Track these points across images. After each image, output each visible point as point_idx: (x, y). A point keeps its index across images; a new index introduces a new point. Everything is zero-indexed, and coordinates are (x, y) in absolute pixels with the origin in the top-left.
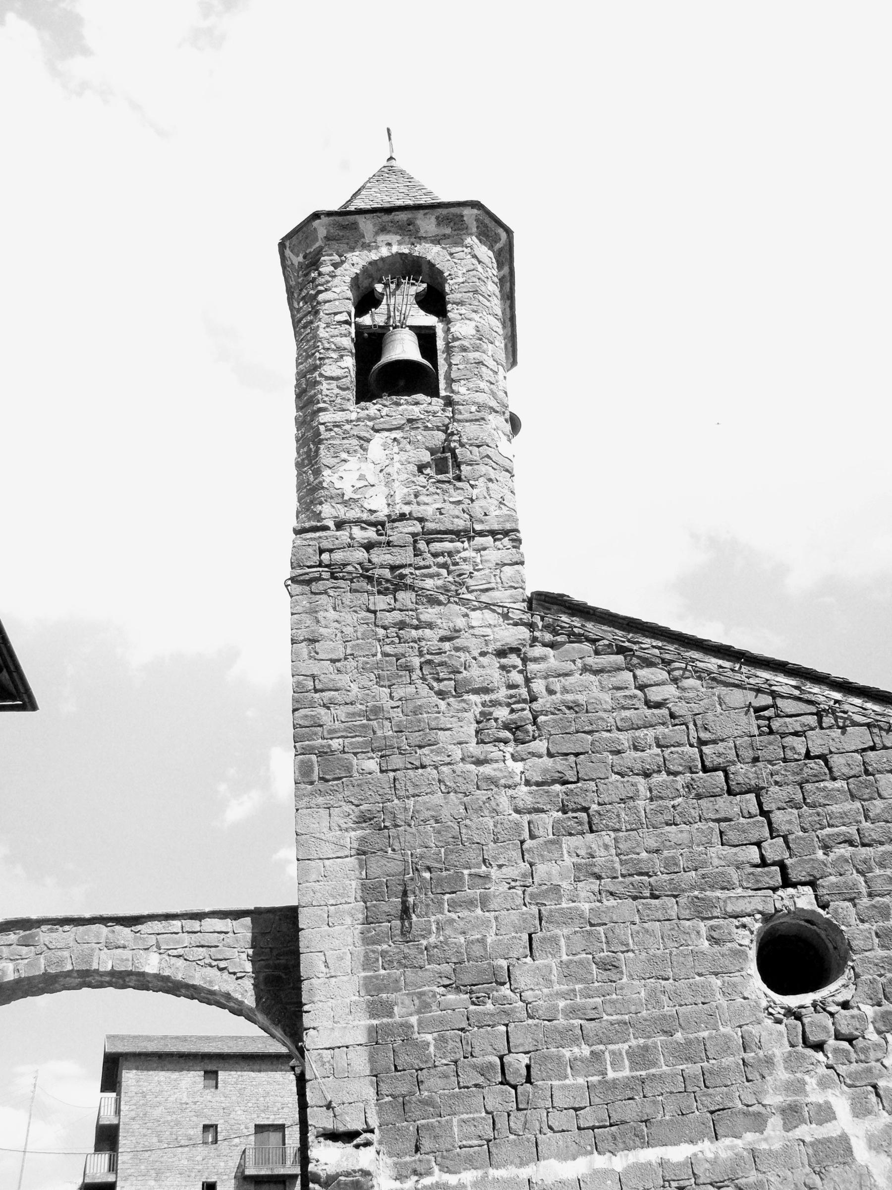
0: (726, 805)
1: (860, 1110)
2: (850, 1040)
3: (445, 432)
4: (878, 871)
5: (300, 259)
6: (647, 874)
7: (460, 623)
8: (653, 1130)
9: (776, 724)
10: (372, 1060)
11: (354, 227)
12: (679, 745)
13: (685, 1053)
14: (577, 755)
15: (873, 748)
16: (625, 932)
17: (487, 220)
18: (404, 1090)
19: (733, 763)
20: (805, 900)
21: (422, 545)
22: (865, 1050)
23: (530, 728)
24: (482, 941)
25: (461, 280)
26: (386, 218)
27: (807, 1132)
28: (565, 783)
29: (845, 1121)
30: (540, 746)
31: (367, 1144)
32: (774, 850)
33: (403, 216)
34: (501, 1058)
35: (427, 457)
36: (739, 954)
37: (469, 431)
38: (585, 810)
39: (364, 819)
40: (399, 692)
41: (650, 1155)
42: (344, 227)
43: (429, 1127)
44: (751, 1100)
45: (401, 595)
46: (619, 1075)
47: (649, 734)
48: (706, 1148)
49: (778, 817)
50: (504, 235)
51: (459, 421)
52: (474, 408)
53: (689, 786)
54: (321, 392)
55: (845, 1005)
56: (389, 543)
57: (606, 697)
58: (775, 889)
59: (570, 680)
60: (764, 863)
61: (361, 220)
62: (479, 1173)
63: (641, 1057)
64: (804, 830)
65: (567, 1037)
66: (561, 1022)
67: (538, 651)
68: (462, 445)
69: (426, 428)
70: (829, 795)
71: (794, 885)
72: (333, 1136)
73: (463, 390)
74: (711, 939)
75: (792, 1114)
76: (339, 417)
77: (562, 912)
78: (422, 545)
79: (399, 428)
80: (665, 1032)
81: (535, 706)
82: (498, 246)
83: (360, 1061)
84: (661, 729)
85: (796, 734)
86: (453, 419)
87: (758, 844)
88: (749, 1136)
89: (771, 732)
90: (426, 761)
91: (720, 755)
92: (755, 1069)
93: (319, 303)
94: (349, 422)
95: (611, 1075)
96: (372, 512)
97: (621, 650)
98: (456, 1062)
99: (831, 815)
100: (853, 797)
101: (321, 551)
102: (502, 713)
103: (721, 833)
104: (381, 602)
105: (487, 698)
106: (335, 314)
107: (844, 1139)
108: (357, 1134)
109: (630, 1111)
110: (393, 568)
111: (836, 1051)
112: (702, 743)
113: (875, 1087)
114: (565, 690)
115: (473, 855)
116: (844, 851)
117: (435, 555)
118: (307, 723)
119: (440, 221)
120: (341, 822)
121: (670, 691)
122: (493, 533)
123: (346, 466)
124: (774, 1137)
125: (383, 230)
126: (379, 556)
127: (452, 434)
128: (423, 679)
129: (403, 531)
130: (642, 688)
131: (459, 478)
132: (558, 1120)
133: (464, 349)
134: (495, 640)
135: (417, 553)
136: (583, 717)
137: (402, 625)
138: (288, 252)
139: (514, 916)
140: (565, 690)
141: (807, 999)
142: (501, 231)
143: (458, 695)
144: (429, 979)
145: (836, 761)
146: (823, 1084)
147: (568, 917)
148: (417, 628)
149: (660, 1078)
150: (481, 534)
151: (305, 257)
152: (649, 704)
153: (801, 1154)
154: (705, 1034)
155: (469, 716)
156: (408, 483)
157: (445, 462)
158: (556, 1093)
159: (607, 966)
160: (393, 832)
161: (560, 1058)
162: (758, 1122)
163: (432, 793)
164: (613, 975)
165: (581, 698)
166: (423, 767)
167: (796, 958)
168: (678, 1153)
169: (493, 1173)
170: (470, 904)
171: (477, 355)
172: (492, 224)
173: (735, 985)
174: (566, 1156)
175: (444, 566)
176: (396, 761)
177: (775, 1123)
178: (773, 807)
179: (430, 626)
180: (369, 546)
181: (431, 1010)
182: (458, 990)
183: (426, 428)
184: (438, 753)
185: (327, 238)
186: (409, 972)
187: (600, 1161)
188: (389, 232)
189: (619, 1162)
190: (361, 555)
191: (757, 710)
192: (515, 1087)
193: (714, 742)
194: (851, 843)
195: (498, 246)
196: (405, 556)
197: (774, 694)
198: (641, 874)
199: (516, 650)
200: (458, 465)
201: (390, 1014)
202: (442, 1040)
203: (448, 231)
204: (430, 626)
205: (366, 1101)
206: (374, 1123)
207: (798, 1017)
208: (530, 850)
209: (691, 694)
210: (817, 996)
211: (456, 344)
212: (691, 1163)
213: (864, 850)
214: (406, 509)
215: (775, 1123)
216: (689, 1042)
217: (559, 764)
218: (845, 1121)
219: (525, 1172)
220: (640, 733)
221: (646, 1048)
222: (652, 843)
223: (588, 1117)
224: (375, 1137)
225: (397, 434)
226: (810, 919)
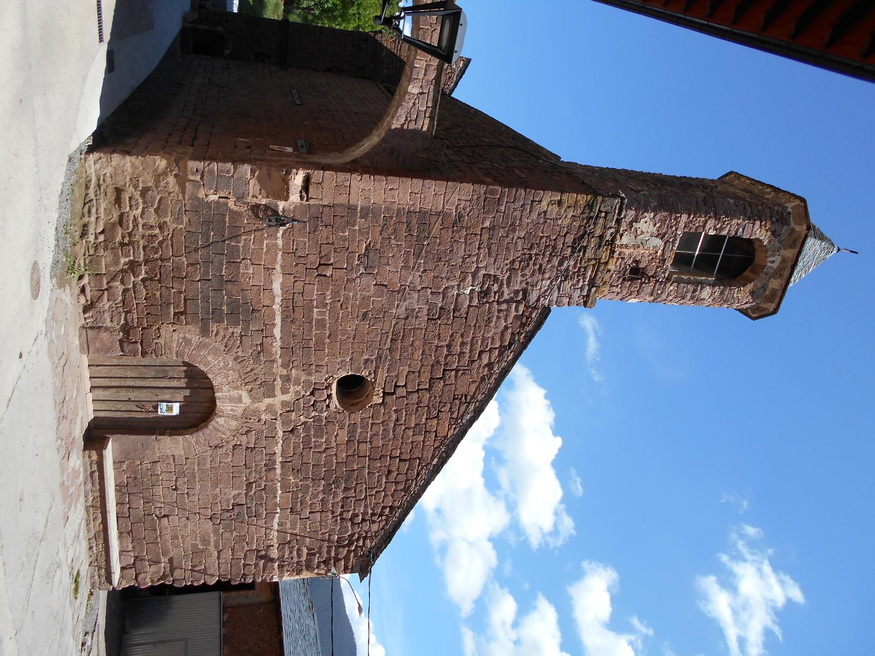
0: (425, 377)
1: (284, 404)
2: (313, 405)
3: (652, 276)
4: (382, 428)
5: (789, 210)
6: (403, 339)
7: (547, 276)
8: (289, 323)
9: (457, 402)
10: (341, 205)
11: (793, 246)
12: (459, 361)
13: (320, 343)
14: (466, 318)
15: (436, 436)
16: (379, 326)
17: (764, 313)
18: (324, 218)
19: (445, 382)
20: (377, 400)
21: (593, 262)
22: (308, 410)
23: (485, 300)
24: (388, 264)
25: (735, 295)
26: (789, 265)
27: (279, 382)
28: (454, 310)
29: (280, 398)
30: (475, 302)
31: (301, 198)
32: (401, 392)
33: (786, 274)
34: (331, 264)
35: (641, 266)
36: (359, 370)
37: (648, 288)
38: (439, 318)
39: (460, 217)
40: (520, 242)
41: (278, 320)
42: (795, 240)
43: (305, 228)
44: (295, 364)
45: (570, 250)
46: (315, 314)
47: (467, 349)
48: (278, 344)
49: (415, 396)
50: (754, 316)
51: (655, 284)
52: (659, 292)
53: (438, 362)
54: (700, 217)
55: (328, 406)
56: (599, 247)
57: (490, 335)
58: (384, 389)
59: (503, 321)
60: (396, 386)
61: (795, 251)
62: (281, 247)
63: (321, 323)
64: (407, 404)
65: (335, 294)
66: (342, 292)
67: (521, 308)
68: (641, 284)
69: (658, 267)
70: (421, 416)
71: (383, 397)
72: (307, 180)
73: (671, 288)
74: (367, 360)
75: (287, 379)
76: (682, 225)
77: (393, 302)
78: (593, 262)
79: (663, 255)
80: (330, 335)
81: (495, 303)
82: (749, 311)
83: (342, 199)
84: (468, 355)
85: (451, 408)
86: (657, 281)
87: (405, 386)
88: (280, 361)
89: (454, 399)
90: (482, 251)
91: (450, 378)
92: (307, 368)
93: (755, 220)
94: (676, 229)
95: (315, 310)
96: (621, 236)
97: (510, 344)
98: (333, 243)
99: (411, 415)
100: (416, 425)
101: (606, 213)
102: (495, 288)
103: (414, 372)
104: (569, 239)
105: (505, 282)
106: (744, 229)
107: (274, 396)
108: (307, 193)
109: (299, 314)
110: (585, 248)
111: (310, 400)
112: (457, 371)
113: (293, 411)
114: (498, 318)
115: (431, 265)
116: (394, 417)
117: (585, 268)
118: (517, 195)
119: (774, 291)
120: (462, 206)
121: (485, 361)
122: (588, 296)
123: (652, 225)
124: (279, 370)
125: (784, 261)
126: (594, 242)
127: (649, 280)
128: (523, 254)
129: (604, 255)
130: (490, 350)
131: (624, 280)
132: (299, 285)
133: (695, 291)
134: (533, 290)
135: (589, 260)
136: (483, 324)
137: (554, 247)
138: (797, 202)
139: (396, 280)
140: (498, 318)
141: (334, 392)
142: (757, 315)
143: (510, 269)
144: (375, 236)
145: (435, 422)
146: (297, 393)
147: (391, 304)
148: (550, 254)
149: (310, 330)
150: (589, 290)
151: (789, 213)
152: (481, 352)
153: (270, 378)
154: (326, 351)
155: (498, 273)
156: (630, 256)
157: (636, 273)
158: (311, 286)
159: (365, 315)
160: (450, 230)
161: (327, 290)
162: (285, 366)
163: (465, 251)
164: (361, 317)
165: (492, 324)
166: (479, 249)
167: (352, 388)
168: (277, 332)
169: (280, 253)
170: (406, 261)
171: (689, 297)
172: (762, 313)
173: (345, 366)
174: (282, 284)
175: (579, 270)
176: (486, 237)
177: (285, 372)
178: (420, 394)
179: (549, 261)
180: (601, 237)
181: (359, 236)
182: (366, 249)
183: (658, 267)
184: (484, 257)
185: (793, 230)
186: (380, 228)
187: (278, 300)
188: (781, 263)
189: (276, 307)
190: (598, 232)
191: (466, 396)
192: (317, 268)
193: (456, 376)
194: (397, 420)
195: (749, 311)
196: (590, 254)
197: (469, 403)
198: (403, 336)
199: (525, 297)
200: (631, 280)
201: (361, 217)
202: (345, 239)
203: (767, 293)
204: (549, 261)
205: (321, 199)
206: (311, 202)
207: (326, 388)
208: (426, 291)
209: (481, 371)
210: (334, 396)
211: (699, 289)
212: (273, 336)
213: (393, 425)
214: (616, 255)
215: (285, 372)
216: (324, 344)
217: (463, 311)
218: (280, 398)
219: (278, 267)
220: (468, 347)
221: (325, 326)
222: (416, 343)
223: (298, 298)
224: (304, 202)
225: (660, 252)
226: (369, 397)
